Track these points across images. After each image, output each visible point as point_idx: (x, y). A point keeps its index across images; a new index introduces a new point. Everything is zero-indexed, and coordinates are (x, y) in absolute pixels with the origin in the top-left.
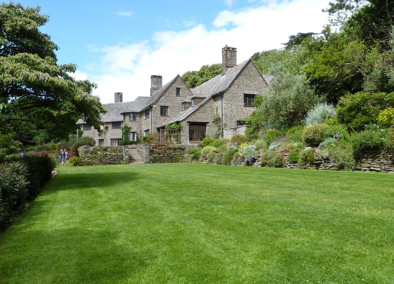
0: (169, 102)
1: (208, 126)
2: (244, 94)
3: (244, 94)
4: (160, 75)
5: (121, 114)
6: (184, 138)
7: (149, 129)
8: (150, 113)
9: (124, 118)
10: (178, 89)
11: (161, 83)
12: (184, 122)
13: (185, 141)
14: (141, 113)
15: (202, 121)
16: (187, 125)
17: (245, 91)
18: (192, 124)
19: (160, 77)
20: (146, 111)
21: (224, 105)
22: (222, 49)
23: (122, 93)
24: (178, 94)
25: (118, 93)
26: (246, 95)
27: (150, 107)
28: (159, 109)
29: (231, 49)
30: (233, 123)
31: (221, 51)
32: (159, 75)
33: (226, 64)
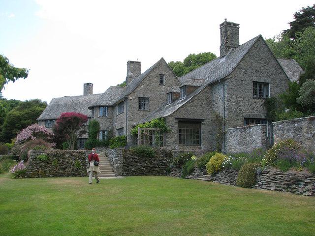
0: (149, 92)
1: (204, 124)
2: (253, 82)
3: (253, 82)
4: (138, 61)
5: (89, 108)
6: (170, 141)
7: (123, 128)
8: (125, 107)
9: (93, 112)
10: (162, 76)
11: (139, 70)
12: (171, 119)
13: (172, 145)
14: (113, 107)
15: (196, 118)
16: (175, 123)
17: (254, 78)
18: (182, 122)
19: (139, 63)
20: (121, 103)
21: (226, 95)
22: (221, 25)
23: (92, 84)
24: (162, 82)
25: (88, 84)
26: (255, 83)
27: (126, 99)
28: (137, 101)
29: (232, 25)
30: (239, 121)
31: (219, 27)
32: (137, 61)
33: (226, 43)
